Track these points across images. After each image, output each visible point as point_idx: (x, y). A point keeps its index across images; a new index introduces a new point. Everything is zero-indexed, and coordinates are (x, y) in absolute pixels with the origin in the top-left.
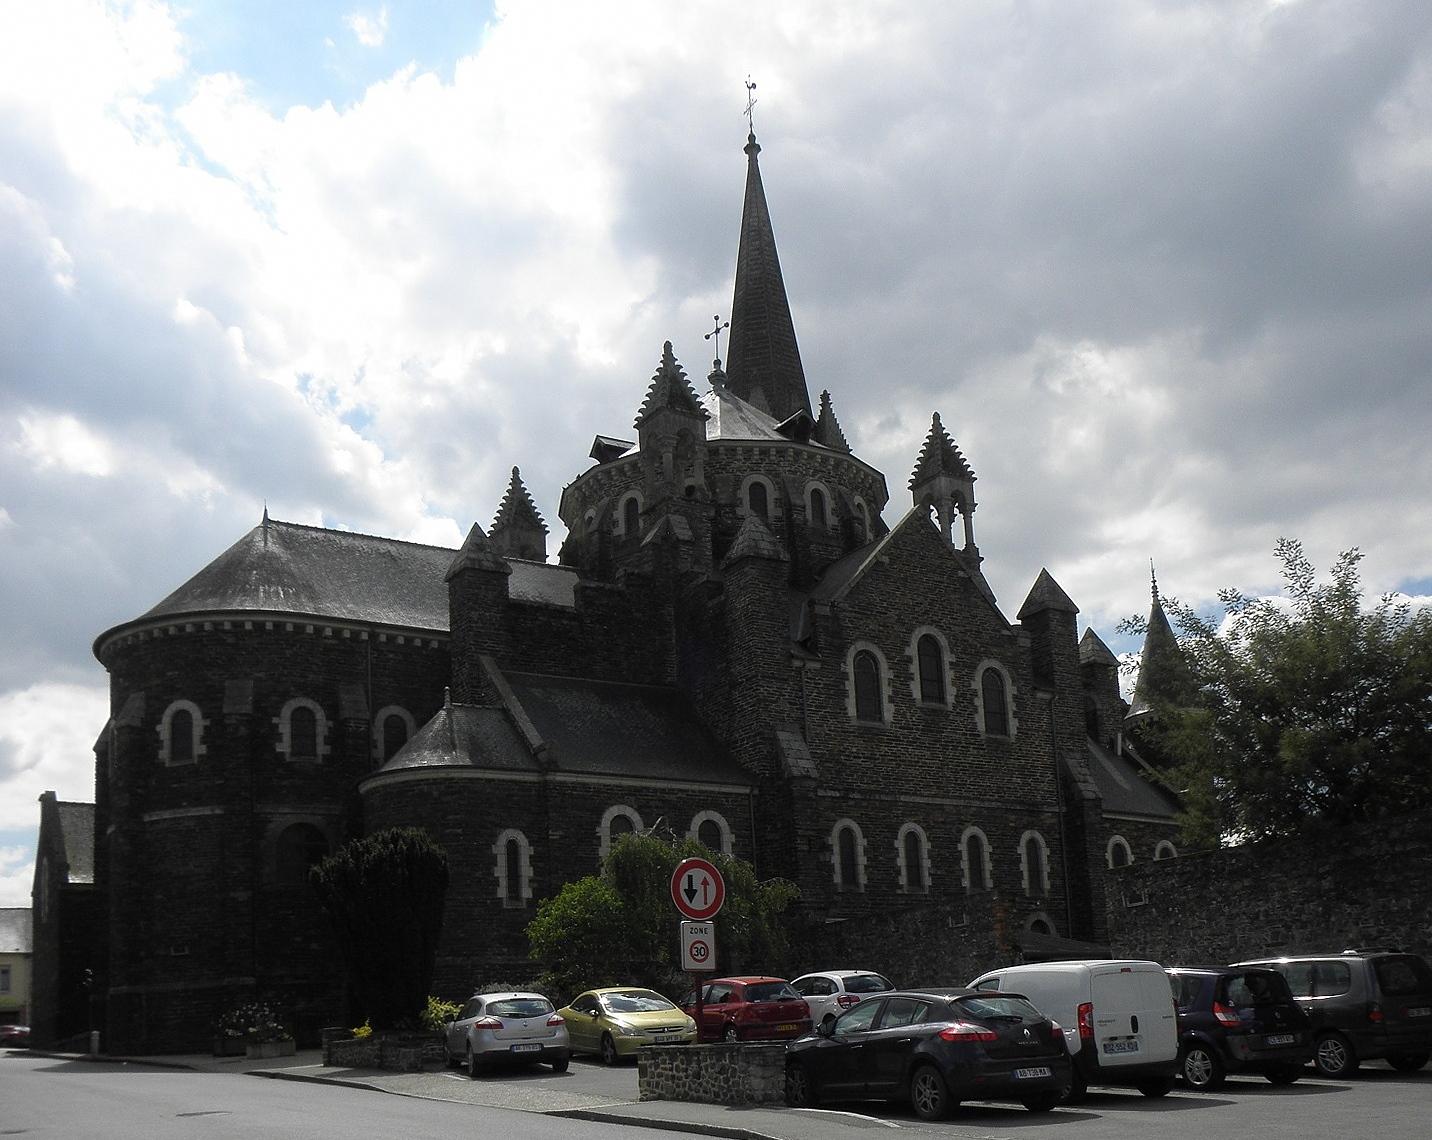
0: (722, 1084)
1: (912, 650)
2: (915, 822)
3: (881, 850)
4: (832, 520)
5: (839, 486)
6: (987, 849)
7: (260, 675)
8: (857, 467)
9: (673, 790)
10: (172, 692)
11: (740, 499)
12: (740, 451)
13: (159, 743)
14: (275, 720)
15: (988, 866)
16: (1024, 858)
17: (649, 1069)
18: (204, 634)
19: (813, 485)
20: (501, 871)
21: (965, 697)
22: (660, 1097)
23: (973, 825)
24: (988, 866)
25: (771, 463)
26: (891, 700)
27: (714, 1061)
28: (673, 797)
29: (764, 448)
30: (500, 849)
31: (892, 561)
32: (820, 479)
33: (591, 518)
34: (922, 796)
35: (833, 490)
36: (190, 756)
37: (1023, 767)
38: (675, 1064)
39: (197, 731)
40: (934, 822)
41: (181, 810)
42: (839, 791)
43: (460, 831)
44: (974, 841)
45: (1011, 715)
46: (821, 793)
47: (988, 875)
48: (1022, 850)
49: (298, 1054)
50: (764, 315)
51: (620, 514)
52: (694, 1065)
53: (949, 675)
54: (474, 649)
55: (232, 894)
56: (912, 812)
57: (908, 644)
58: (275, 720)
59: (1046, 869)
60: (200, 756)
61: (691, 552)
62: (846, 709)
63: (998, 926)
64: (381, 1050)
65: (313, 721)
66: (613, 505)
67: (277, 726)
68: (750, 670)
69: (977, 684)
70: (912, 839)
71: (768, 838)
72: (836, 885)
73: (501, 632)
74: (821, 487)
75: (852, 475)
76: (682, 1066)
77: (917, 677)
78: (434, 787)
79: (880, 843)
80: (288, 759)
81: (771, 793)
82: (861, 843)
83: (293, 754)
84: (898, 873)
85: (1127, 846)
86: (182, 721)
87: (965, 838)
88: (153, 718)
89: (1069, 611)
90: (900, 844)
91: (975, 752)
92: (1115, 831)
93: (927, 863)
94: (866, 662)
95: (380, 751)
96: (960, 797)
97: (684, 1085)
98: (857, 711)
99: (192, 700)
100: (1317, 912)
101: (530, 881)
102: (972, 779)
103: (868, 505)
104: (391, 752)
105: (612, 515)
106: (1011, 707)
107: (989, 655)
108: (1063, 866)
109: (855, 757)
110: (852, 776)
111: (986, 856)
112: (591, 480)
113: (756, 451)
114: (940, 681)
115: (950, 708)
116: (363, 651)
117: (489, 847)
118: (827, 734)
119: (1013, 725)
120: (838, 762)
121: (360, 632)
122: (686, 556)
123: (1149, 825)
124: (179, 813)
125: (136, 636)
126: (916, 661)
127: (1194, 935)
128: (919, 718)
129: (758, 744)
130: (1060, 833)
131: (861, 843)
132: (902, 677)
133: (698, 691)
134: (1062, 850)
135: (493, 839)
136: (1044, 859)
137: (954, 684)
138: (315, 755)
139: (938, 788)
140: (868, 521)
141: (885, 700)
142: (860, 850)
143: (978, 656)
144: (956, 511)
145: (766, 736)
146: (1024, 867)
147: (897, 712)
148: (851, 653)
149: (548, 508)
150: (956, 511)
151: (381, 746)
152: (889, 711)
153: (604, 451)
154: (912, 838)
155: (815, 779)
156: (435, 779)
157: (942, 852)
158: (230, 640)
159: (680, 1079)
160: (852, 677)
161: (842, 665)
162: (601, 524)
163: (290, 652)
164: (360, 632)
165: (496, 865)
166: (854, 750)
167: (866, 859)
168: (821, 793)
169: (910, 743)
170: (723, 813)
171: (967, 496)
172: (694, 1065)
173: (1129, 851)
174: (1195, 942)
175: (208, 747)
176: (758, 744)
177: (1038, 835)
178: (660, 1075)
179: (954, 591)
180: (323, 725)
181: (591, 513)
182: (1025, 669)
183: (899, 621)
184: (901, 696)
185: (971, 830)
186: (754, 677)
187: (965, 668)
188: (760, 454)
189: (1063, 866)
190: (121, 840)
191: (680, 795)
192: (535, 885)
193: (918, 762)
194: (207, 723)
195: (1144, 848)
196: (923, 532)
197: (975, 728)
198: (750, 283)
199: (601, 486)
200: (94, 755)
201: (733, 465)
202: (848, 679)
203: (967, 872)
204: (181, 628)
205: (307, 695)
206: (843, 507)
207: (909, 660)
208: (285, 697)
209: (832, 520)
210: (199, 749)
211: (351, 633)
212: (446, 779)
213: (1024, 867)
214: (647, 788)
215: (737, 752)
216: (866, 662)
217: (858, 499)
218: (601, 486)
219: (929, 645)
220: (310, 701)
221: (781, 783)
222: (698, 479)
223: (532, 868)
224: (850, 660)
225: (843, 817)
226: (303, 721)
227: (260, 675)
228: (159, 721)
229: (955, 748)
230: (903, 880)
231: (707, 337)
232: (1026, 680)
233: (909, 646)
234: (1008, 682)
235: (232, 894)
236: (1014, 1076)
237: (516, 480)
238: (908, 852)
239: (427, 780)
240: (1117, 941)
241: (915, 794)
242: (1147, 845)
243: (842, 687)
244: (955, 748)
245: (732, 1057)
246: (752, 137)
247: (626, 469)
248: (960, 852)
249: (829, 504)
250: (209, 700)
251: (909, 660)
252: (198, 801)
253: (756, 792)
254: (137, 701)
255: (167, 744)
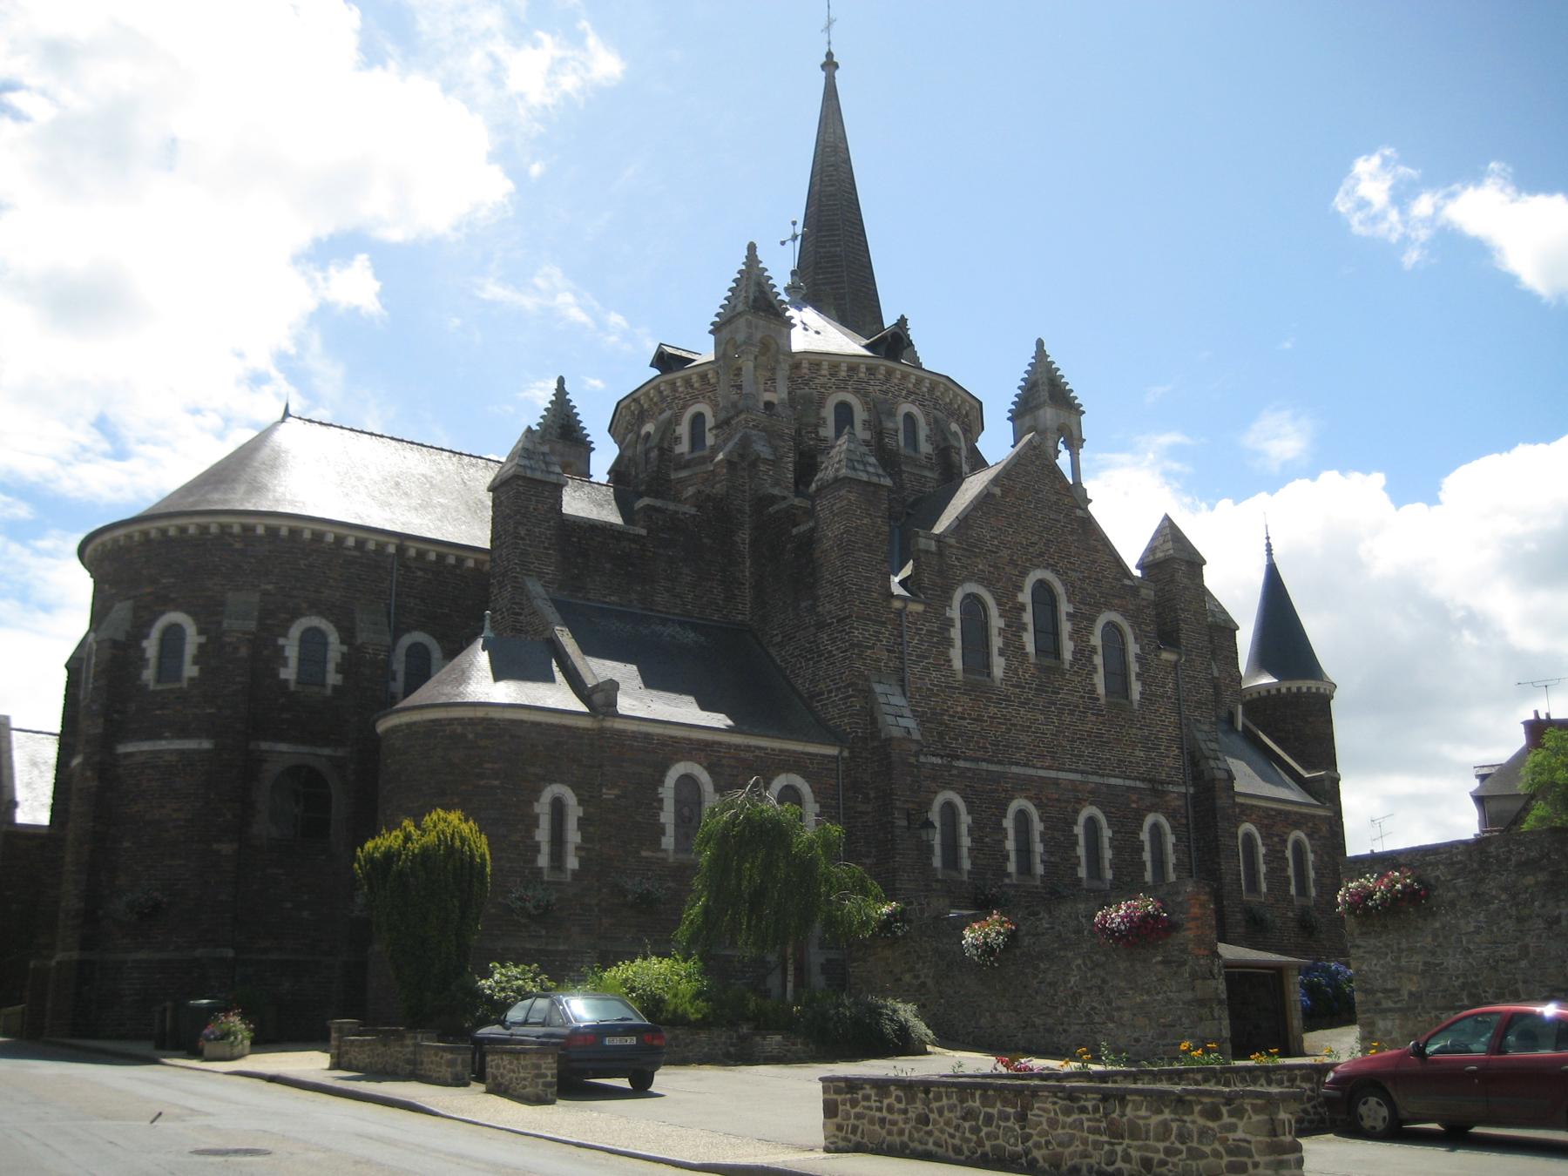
0: (967, 1134)
1: (1025, 597)
2: (1026, 797)
3: (988, 828)
4: (925, 448)
5: (935, 412)
6: (1107, 833)
7: (270, 587)
8: (954, 392)
9: (750, 747)
10: (167, 602)
11: (824, 418)
12: (825, 365)
13: (143, 661)
14: (281, 641)
15: (1108, 854)
16: (1147, 846)
17: (841, 1107)
18: (209, 537)
19: (906, 407)
20: (542, 835)
21: (1084, 653)
22: (858, 1148)
23: (1091, 804)
24: (1108, 854)
25: (860, 381)
26: (1001, 653)
27: (954, 1100)
28: (749, 756)
29: (852, 362)
30: (543, 807)
31: (1005, 494)
32: (913, 402)
33: (648, 434)
34: (1034, 767)
35: (927, 414)
36: (178, 678)
37: (1147, 738)
38: (886, 1102)
39: (190, 649)
40: (1047, 799)
41: (163, 742)
42: (942, 757)
43: (497, 783)
44: (1092, 823)
45: (1133, 677)
46: (922, 759)
47: (1107, 864)
48: (1145, 836)
49: (559, 1102)
50: (837, 232)
51: (683, 429)
52: (918, 1104)
53: (1066, 627)
54: (518, 570)
55: (215, 846)
56: (1024, 786)
57: (1020, 589)
58: (281, 641)
59: (1171, 859)
60: (191, 679)
61: (771, 473)
62: (950, 661)
63: (1191, 925)
64: (414, 1053)
65: (325, 644)
66: (675, 420)
67: (283, 647)
68: (842, 609)
69: (1096, 640)
70: (1022, 818)
71: (859, 809)
72: (936, 869)
73: (551, 552)
74: (915, 410)
75: (948, 400)
76: (897, 1106)
77: (1031, 627)
78: (469, 728)
79: (985, 821)
80: (292, 687)
81: (864, 755)
82: (965, 820)
83: (298, 682)
84: (1006, 858)
85: (1257, 836)
86: (173, 636)
87: (1081, 819)
88: (140, 630)
89: (1195, 563)
90: (1009, 823)
91: (1094, 718)
92: (1245, 818)
93: (1039, 848)
94: (973, 606)
95: (398, 685)
96: (1076, 771)
97: (901, 1132)
98: (963, 665)
99: (188, 613)
100: (979, 927)
101: (577, 848)
102: (1090, 750)
103: (964, 435)
104: (410, 689)
105: (674, 431)
106: (1134, 668)
107: (1110, 607)
108: (1190, 857)
109: (959, 718)
110: (957, 740)
111: (1106, 843)
112: (652, 391)
113: (844, 367)
114: (1056, 634)
115: (1067, 666)
116: (389, 567)
117: (530, 803)
118: (928, 689)
119: (1136, 688)
120: (941, 723)
121: (387, 544)
122: (765, 477)
123: (1279, 812)
124: (162, 745)
125: (129, 537)
126: (1029, 609)
127: (1468, 942)
128: (1033, 675)
129: (851, 696)
130: (1187, 818)
131: (965, 820)
132: (1014, 628)
133: (775, 632)
134: (1189, 838)
135: (536, 794)
136: (1170, 848)
137: (1071, 638)
138: (323, 685)
139: (1053, 758)
140: (964, 453)
141: (995, 651)
142: (964, 829)
143: (1099, 607)
144: (1061, 446)
145: (860, 687)
146: (1147, 856)
147: (1008, 668)
148: (958, 595)
149: (595, 421)
150: (1061, 446)
151: (401, 677)
152: (998, 666)
153: (666, 361)
154: (1022, 816)
155: (918, 742)
156: (470, 719)
157: (1056, 834)
158: (238, 546)
159: (894, 1123)
160: (958, 624)
161: (947, 608)
162: (662, 439)
163: (306, 562)
164: (387, 544)
165: (538, 827)
166: (959, 709)
167: (970, 839)
168: (922, 759)
169: (1022, 704)
170: (806, 776)
171: (1075, 432)
172: (918, 1104)
173: (1259, 842)
174: (1469, 951)
175: (201, 669)
176: (851, 696)
177: (1162, 820)
178: (859, 1116)
179: (1072, 532)
180: (335, 648)
181: (649, 427)
182: (1148, 625)
183: (1012, 562)
184: (1013, 648)
185: (1088, 811)
186: (847, 617)
187: (1084, 623)
188: (848, 371)
189: (1190, 857)
190: (89, 774)
191: (757, 753)
192: (583, 854)
193: (1030, 727)
194: (203, 639)
195: (1276, 839)
196: (1037, 463)
197: (1093, 691)
198: (823, 199)
199: (663, 399)
200: (65, 673)
201: (817, 381)
202: (953, 626)
203: (1083, 860)
204: (183, 530)
205: (321, 614)
206: (939, 429)
207: (1022, 608)
208: (296, 614)
209: (925, 448)
210: (190, 670)
211: (377, 545)
212: (483, 719)
213: (1147, 856)
214: (720, 743)
215: (822, 705)
216: (973, 606)
217: (954, 427)
218: (663, 399)
219: (1044, 593)
220: (324, 621)
221: (876, 744)
222: (779, 395)
223: (579, 833)
224: (1028, 589)
225: (944, 788)
226: (313, 643)
227: (270, 587)
228: (146, 636)
229: (1072, 713)
230: (1012, 867)
231: (783, 243)
232: (1150, 637)
233: (1022, 591)
234: (1130, 639)
235: (215, 846)
236: (602, 1042)
237: (561, 390)
238: (1017, 832)
239: (463, 719)
240: (1358, 947)
241: (1026, 765)
242: (1278, 835)
243: (946, 635)
244: (1072, 713)
245: (984, 1097)
246: (829, 55)
247: (678, 384)
248: (1077, 836)
249: (923, 431)
250: (208, 615)
251: (1022, 608)
252: (183, 732)
253: (846, 754)
254: (122, 611)
255: (153, 662)
